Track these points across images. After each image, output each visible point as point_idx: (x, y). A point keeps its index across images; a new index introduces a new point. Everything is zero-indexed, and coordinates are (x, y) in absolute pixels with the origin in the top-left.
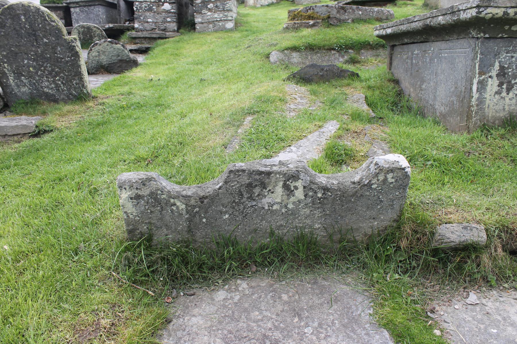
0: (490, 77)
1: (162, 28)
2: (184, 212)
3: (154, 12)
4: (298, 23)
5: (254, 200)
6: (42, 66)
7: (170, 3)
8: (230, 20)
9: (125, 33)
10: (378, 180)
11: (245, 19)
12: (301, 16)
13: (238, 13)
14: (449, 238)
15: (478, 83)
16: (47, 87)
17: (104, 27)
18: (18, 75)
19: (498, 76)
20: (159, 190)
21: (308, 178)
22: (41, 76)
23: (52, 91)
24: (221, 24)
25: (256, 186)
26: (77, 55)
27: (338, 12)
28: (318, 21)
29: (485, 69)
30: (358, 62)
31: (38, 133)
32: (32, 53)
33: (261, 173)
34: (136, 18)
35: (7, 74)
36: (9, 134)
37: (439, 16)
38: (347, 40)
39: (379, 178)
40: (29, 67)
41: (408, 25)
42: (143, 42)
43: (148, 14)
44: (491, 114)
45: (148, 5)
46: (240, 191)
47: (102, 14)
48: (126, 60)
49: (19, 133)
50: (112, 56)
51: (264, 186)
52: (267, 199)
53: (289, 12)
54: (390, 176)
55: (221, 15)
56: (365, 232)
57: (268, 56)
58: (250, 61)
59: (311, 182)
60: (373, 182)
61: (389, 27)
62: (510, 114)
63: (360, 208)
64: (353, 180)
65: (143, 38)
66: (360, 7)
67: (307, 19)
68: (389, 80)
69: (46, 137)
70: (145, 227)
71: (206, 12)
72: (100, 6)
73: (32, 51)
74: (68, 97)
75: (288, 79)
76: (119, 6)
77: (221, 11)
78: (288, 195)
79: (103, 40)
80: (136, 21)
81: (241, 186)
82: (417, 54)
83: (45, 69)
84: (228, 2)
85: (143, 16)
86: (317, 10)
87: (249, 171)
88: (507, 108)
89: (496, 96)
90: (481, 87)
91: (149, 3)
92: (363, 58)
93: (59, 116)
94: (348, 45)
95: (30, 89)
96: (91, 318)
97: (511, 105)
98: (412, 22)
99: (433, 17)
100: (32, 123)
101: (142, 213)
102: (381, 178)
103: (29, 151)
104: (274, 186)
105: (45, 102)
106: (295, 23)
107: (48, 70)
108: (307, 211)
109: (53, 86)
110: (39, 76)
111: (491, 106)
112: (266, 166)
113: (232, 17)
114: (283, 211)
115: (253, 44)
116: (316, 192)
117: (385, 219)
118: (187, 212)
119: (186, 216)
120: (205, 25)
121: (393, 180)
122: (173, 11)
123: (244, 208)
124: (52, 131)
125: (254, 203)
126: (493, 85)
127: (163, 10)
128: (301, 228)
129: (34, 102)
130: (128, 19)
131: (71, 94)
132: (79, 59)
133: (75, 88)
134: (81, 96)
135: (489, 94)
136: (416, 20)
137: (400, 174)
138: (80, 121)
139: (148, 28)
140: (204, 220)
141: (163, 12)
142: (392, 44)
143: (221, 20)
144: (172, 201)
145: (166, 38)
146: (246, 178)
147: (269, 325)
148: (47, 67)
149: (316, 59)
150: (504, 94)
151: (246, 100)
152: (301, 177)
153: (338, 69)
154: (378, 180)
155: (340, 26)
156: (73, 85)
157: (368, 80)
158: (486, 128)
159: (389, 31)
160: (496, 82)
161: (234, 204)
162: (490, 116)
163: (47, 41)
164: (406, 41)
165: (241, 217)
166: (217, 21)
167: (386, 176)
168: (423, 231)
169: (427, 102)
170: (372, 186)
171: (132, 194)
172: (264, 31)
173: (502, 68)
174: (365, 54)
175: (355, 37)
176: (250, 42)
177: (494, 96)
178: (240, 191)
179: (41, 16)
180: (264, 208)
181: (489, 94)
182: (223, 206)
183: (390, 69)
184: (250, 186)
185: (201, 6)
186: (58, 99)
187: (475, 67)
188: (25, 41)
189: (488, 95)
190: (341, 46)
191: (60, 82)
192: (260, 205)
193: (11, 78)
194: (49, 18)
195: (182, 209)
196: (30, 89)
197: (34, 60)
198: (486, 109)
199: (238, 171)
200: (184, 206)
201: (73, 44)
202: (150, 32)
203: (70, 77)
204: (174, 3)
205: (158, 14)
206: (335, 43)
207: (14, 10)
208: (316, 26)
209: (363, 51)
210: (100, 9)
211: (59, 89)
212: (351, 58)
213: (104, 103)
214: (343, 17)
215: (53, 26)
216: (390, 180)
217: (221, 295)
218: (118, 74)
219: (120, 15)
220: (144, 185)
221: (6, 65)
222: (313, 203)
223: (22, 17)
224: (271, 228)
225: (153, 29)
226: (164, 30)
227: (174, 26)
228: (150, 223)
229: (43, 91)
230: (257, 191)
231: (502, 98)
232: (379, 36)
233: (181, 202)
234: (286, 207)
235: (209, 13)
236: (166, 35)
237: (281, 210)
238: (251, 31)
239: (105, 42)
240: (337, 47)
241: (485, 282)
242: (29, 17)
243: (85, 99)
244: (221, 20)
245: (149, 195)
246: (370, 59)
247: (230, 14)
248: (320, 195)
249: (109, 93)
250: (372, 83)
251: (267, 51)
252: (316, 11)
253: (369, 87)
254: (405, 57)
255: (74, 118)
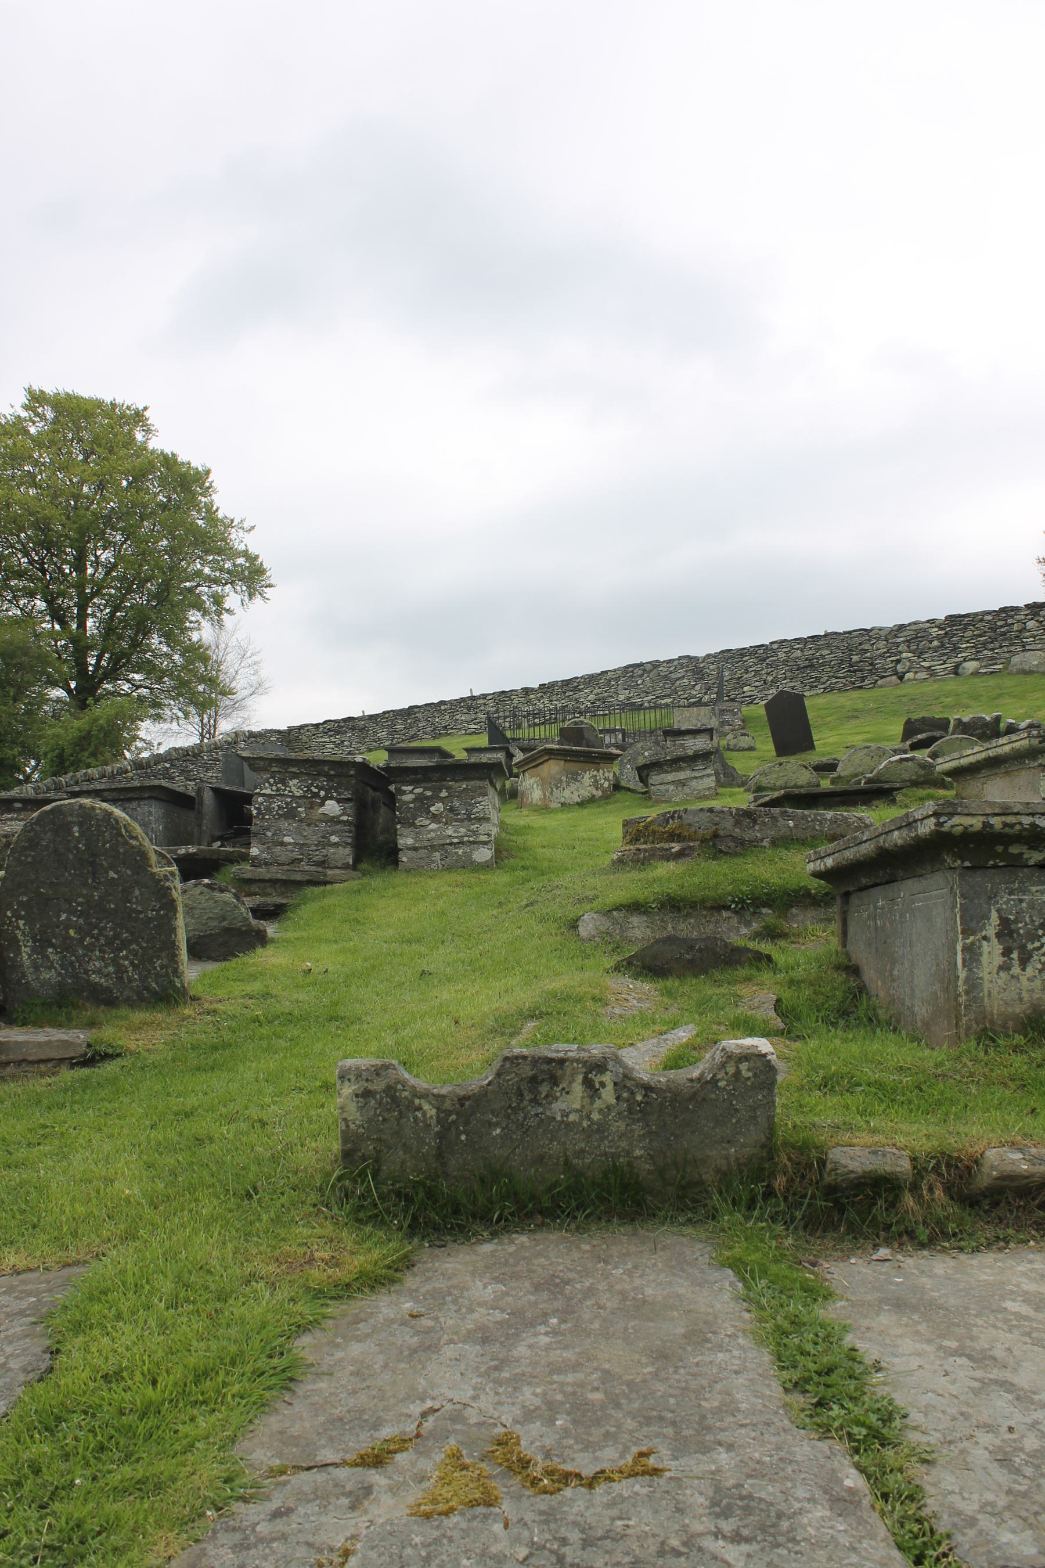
0: (985, 938)
1: (316, 859)
2: (434, 1122)
3: (301, 821)
4: (645, 850)
5: (540, 1105)
6: (96, 927)
7: (339, 801)
8: (485, 843)
9: (223, 870)
10: (726, 1073)
11: (520, 840)
12: (654, 832)
13: (502, 825)
14: (845, 1167)
15: (962, 951)
16: (99, 972)
17: (175, 852)
18: (42, 943)
19: (998, 935)
20: (399, 1082)
21: (621, 1070)
22: (90, 948)
23: (107, 981)
24: (460, 852)
25: (543, 1080)
26: (170, 906)
27: (737, 823)
28: (692, 844)
29: (973, 924)
30: (783, 935)
31: (92, 1058)
32: (80, 900)
33: (549, 1061)
34: (256, 834)
35: (19, 941)
36: (31, 1058)
37: (893, 830)
38: (756, 887)
39: (728, 1070)
40: (67, 928)
41: (856, 848)
42: (269, 890)
43: (284, 824)
44: (996, 1008)
45: (287, 804)
46: (519, 1088)
47: (157, 820)
48: (239, 930)
49: (52, 1057)
50: (209, 918)
51: (554, 1081)
52: (559, 1103)
53: (626, 824)
54: (744, 1066)
55: (463, 830)
56: (716, 1166)
57: (573, 925)
58: (533, 935)
59: (625, 1076)
60: (719, 1076)
61: (829, 855)
62: (1035, 1007)
63: (703, 1122)
64: (689, 1077)
65: (270, 881)
66: (790, 810)
67: (667, 841)
68: (838, 968)
69: (109, 1068)
70: (371, 1147)
71: (428, 822)
72: (153, 802)
73: (82, 896)
74: (139, 994)
75: (617, 968)
76: (201, 803)
77: (462, 821)
78: (591, 1097)
79: (193, 881)
80: (254, 842)
81: (522, 1080)
82: (883, 908)
83: (100, 934)
84: (480, 799)
85: (273, 829)
86: (689, 818)
87: (533, 1057)
88: (1025, 996)
89: (1002, 974)
90: (970, 958)
91: (289, 800)
92: (795, 925)
93: (127, 1029)
94: (758, 898)
95: (60, 974)
96: (300, 1251)
97: (1033, 991)
98: (861, 843)
99: (887, 833)
100: (78, 1037)
101: (370, 1121)
102: (731, 1070)
103: (85, 1083)
104: (570, 1083)
105: (87, 1004)
106: (639, 850)
107: (106, 937)
108: (621, 1125)
109: (111, 969)
110: (85, 948)
111: (994, 993)
112: (558, 1052)
113: (489, 835)
114: (585, 1124)
115: (539, 899)
116: (633, 1093)
117: (746, 1144)
118: (438, 1122)
119: (436, 1129)
120: (423, 853)
121: (750, 1074)
122: (345, 818)
123: (525, 1118)
124: (119, 1055)
125: (540, 1110)
126: (992, 953)
127: (322, 817)
128: (613, 1155)
129: (68, 1000)
130: (218, 834)
131: (147, 988)
132: (175, 914)
133: (158, 975)
134: (167, 995)
135: (986, 971)
136: (865, 839)
137: (759, 1064)
138: (174, 1041)
139: (283, 859)
140: (463, 1137)
141: (322, 821)
142: (843, 890)
143: (462, 843)
144: (417, 1101)
145: (325, 883)
146: (528, 1068)
147: (561, 1268)
148: (105, 928)
149: (686, 928)
150: (1016, 970)
151: (525, 997)
152: (610, 1067)
153: (726, 945)
154: (726, 1073)
155: (744, 856)
156: (155, 968)
157: (793, 968)
158: (988, 1033)
159: (829, 862)
160: (998, 948)
161: (509, 1111)
162: (995, 1012)
163: (116, 876)
164: (864, 881)
165: (519, 1133)
166: (451, 844)
167: (737, 1067)
168: (810, 1161)
169: (903, 1004)
170: (720, 1084)
171: (359, 1088)
172: (566, 869)
173: (1004, 922)
174: (800, 918)
175: (775, 880)
176: (533, 894)
177: (997, 974)
178: (519, 1088)
179: (113, 828)
180: (554, 1118)
181: (986, 971)
182: (493, 1112)
183: (844, 945)
184: (534, 1081)
185: (415, 808)
186: (117, 998)
187: (956, 922)
188: (70, 875)
189: (986, 973)
190: (742, 901)
191: (127, 963)
192: (548, 1113)
193: (27, 949)
194: (127, 831)
195: (431, 1117)
196: (60, 974)
197: (82, 914)
198: (986, 1000)
199: (517, 1058)
200: (434, 1112)
201: (167, 884)
202: (286, 868)
203: (151, 951)
204: (348, 800)
205: (309, 825)
206: (729, 894)
207: (63, 814)
208: (687, 855)
209: (794, 911)
210: (152, 810)
211: (122, 978)
212: (766, 927)
213: (215, 1011)
214: (749, 835)
215: (133, 847)
216: (746, 1074)
217: (487, 1248)
218: (216, 961)
219: (200, 826)
220: (378, 1074)
221: (21, 922)
222: (630, 1111)
223: (76, 829)
224: (565, 1154)
225: (295, 861)
226: (322, 864)
227: (345, 854)
228: (379, 1140)
229: (88, 981)
230: (544, 1089)
231: (1013, 977)
232: (817, 875)
233: (430, 1103)
234: (588, 1117)
235: (433, 826)
236: (325, 875)
237: (580, 1124)
238: (535, 868)
239: (196, 885)
240: (733, 901)
241: (905, 1236)
242: (89, 829)
243: (175, 1000)
244: (462, 843)
245: (384, 1091)
246: (810, 928)
247: (484, 827)
248: (639, 1098)
249: (221, 993)
250: (799, 973)
251: (572, 912)
252: (686, 822)
253: (792, 982)
254: (865, 915)
255: (161, 1037)
